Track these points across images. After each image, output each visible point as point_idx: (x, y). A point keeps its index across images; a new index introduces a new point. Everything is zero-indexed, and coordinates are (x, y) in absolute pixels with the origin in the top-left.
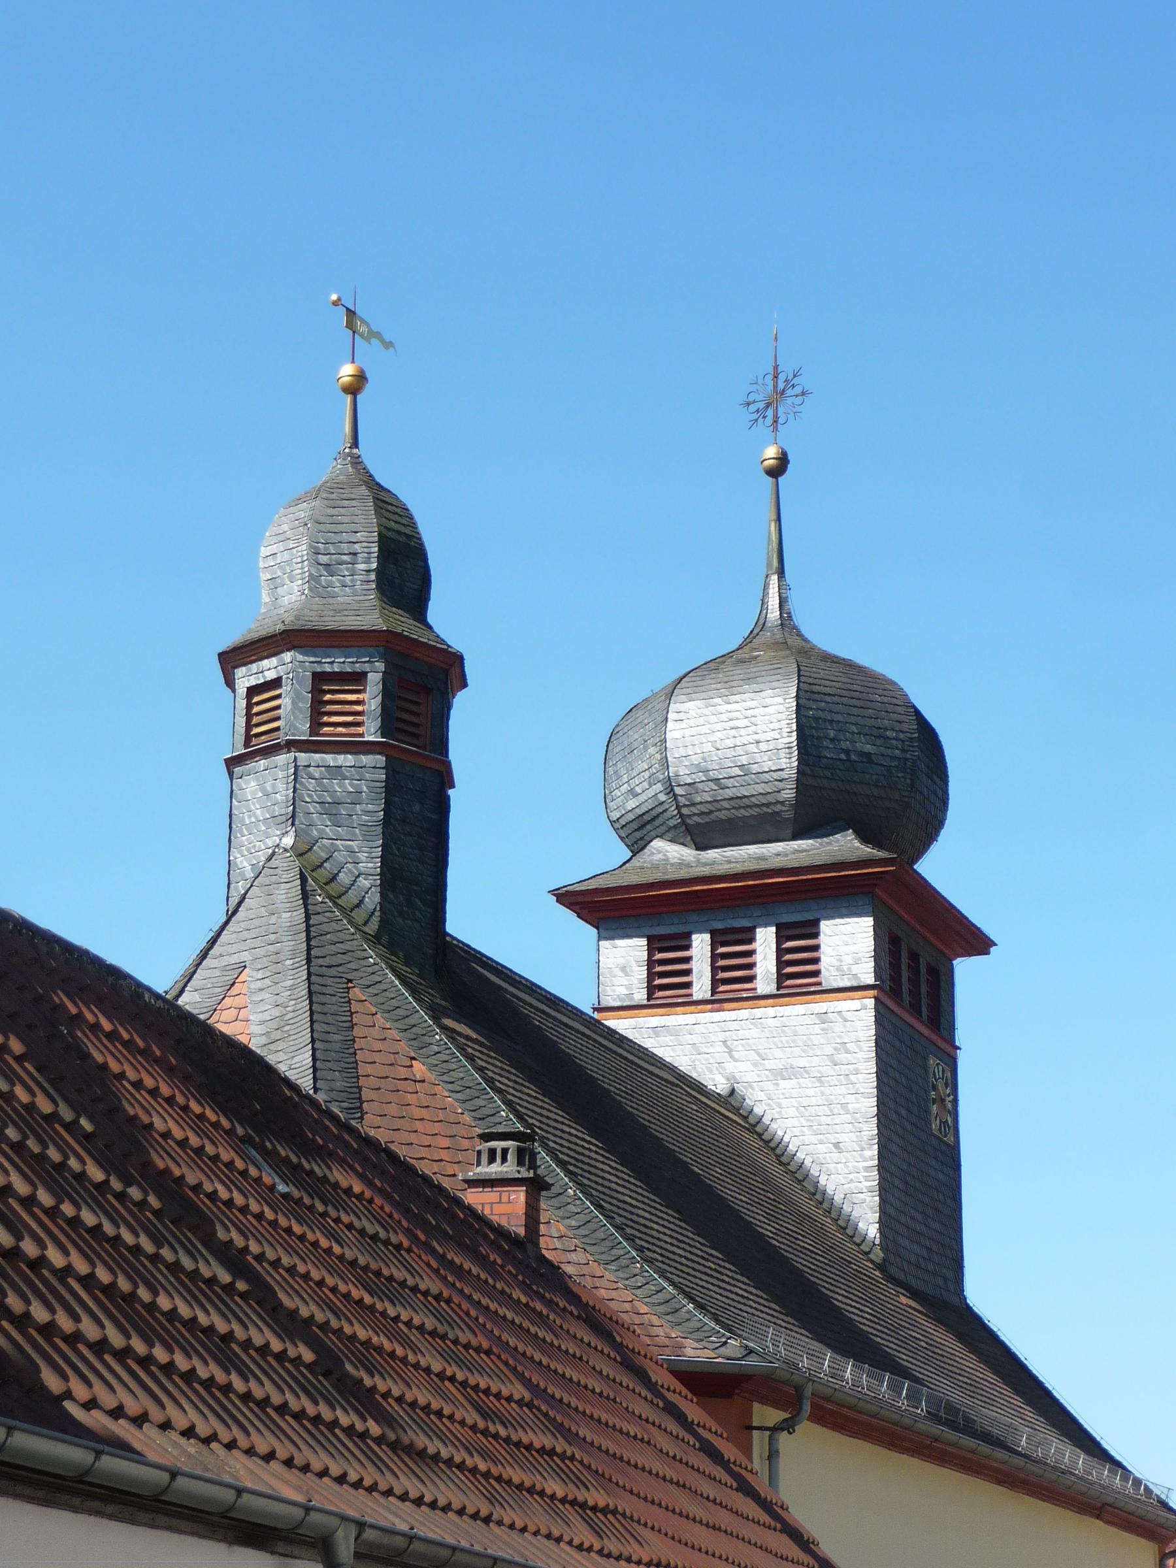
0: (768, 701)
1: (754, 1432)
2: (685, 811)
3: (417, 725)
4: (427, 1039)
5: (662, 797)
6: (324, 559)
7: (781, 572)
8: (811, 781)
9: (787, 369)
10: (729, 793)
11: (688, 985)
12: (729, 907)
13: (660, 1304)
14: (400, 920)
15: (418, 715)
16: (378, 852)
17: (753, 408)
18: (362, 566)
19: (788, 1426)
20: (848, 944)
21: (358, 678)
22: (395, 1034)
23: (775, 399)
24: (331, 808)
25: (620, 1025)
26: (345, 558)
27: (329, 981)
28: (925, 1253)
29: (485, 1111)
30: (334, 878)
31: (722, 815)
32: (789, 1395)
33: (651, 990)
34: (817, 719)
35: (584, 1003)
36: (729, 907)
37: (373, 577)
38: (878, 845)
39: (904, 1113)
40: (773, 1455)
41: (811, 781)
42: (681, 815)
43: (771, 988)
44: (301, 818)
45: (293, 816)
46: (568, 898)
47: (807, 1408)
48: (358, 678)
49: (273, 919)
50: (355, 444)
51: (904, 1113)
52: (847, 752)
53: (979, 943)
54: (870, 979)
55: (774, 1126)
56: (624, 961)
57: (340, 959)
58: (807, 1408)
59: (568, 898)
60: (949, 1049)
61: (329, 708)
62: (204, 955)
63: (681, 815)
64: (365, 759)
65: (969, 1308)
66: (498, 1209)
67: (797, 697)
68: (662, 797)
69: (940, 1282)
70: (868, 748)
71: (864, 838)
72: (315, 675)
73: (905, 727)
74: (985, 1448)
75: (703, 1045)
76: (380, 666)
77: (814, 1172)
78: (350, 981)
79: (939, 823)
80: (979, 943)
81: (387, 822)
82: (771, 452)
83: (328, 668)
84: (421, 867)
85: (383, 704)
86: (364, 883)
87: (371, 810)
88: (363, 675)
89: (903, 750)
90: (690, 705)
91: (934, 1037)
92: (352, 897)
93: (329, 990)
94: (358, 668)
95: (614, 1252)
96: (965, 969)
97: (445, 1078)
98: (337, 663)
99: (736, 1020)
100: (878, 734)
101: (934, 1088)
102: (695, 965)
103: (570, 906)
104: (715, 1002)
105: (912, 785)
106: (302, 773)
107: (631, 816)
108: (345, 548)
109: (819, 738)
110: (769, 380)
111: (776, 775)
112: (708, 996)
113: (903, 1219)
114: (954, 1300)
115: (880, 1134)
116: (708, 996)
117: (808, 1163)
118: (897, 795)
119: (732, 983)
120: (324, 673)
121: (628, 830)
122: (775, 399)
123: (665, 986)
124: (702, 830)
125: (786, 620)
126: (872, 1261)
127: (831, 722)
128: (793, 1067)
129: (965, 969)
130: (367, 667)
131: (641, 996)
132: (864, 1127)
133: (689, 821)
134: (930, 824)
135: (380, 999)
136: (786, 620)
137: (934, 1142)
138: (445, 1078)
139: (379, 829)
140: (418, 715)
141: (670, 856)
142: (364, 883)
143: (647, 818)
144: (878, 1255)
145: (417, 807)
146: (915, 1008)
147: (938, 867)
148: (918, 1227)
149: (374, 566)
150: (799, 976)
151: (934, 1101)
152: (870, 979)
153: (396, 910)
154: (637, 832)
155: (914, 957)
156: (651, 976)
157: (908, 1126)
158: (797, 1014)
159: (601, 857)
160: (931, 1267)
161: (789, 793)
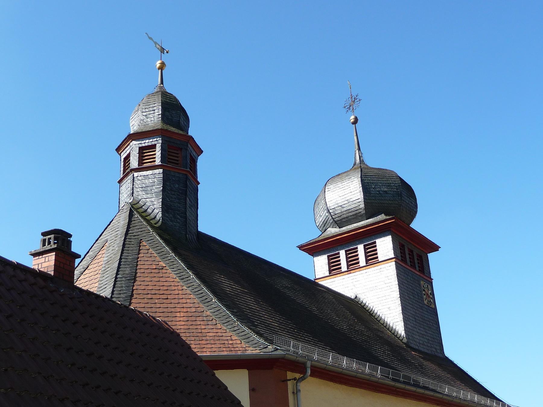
0: (352, 180)
1: (288, 382)
2: (333, 217)
3: (178, 161)
4: (167, 255)
5: (327, 214)
6: (144, 114)
7: (359, 149)
8: (369, 201)
9: (354, 95)
10: (345, 209)
11: (340, 268)
12: (347, 241)
13: (242, 336)
14: (171, 223)
15: (178, 157)
16: (161, 200)
17: (346, 108)
18: (157, 114)
19: (302, 379)
20: (385, 246)
21: (154, 146)
22: (155, 255)
23: (352, 103)
24: (145, 189)
25: (322, 283)
26: (152, 112)
27: (133, 240)
28: (426, 341)
29: (184, 277)
30: (146, 211)
31: (345, 216)
32: (298, 366)
33: (330, 271)
34: (368, 183)
35: (313, 279)
36: (347, 241)
37: (160, 116)
38: (389, 215)
39: (412, 297)
40: (296, 393)
41: (369, 201)
42: (333, 218)
43: (364, 264)
44: (135, 193)
45: (133, 193)
46: (301, 247)
47: (309, 372)
48: (154, 146)
49: (119, 224)
50: (162, 83)
51: (412, 297)
52: (379, 191)
53: (435, 248)
54: (393, 256)
55: (369, 305)
56: (321, 264)
57: (139, 233)
58: (309, 372)
59: (301, 247)
60: (430, 280)
61: (146, 158)
62: (97, 240)
63: (333, 218)
64: (157, 171)
65: (447, 358)
66: (45, 265)
67: (361, 177)
68: (327, 214)
69: (434, 350)
70: (386, 189)
71: (386, 215)
72: (140, 148)
73: (397, 182)
74: (432, 393)
75: (345, 285)
76: (160, 141)
77: (383, 318)
78: (141, 240)
79: (416, 212)
80: (435, 248)
81: (163, 191)
82: (352, 117)
83: (144, 145)
84: (179, 205)
85: (161, 153)
86: (156, 211)
87: (158, 188)
88: (155, 145)
89: (397, 189)
90: (331, 186)
91: (422, 275)
92: (152, 216)
93: (132, 243)
94: (153, 143)
95: (227, 319)
96: (431, 256)
97: (171, 267)
98: (147, 142)
99: (357, 275)
100: (389, 186)
101: (424, 291)
102: (342, 262)
103: (303, 250)
104: (349, 271)
105: (401, 198)
106: (135, 179)
107: (321, 223)
108: (151, 109)
109: (369, 188)
110: (350, 99)
111: (358, 201)
112: (346, 270)
113: (415, 330)
114: (441, 355)
115: (402, 303)
116: (346, 270)
117: (381, 315)
118: (397, 202)
119: (353, 264)
120: (143, 147)
121: (322, 228)
122: (352, 103)
123: (334, 268)
124: (340, 223)
125: (362, 161)
126: (402, 342)
127: (373, 183)
128: (374, 286)
129: (431, 256)
130: (156, 142)
131: (327, 274)
132: (396, 301)
133: (335, 220)
134: (412, 212)
135: (151, 244)
136: (362, 161)
137: (427, 307)
138: (171, 267)
139: (161, 193)
140: (178, 157)
141: (333, 231)
142: (156, 211)
143: (325, 222)
144: (405, 340)
145: (177, 186)
146: (413, 266)
147: (417, 225)
148: (422, 333)
149: (160, 113)
150: (372, 258)
151: (424, 295)
152: (393, 256)
153: (176, 223)
154: (324, 227)
155: (411, 251)
156: (330, 267)
157: (414, 301)
158: (373, 270)
159: (313, 234)
160: (429, 345)
161: (362, 206)
